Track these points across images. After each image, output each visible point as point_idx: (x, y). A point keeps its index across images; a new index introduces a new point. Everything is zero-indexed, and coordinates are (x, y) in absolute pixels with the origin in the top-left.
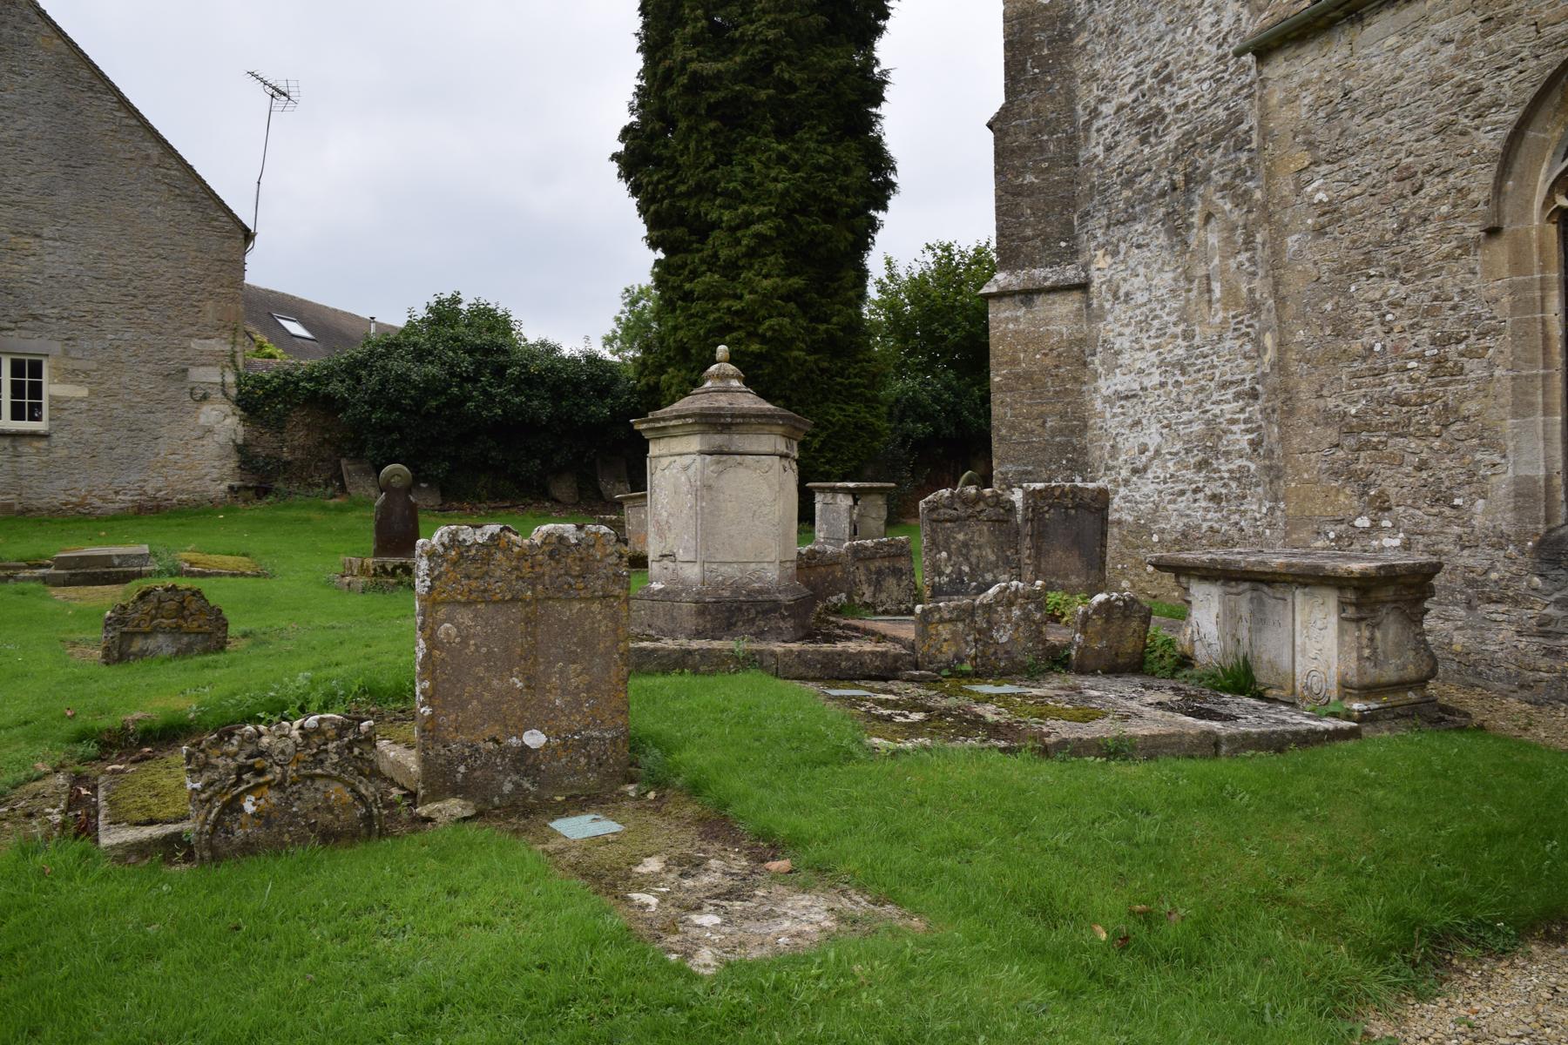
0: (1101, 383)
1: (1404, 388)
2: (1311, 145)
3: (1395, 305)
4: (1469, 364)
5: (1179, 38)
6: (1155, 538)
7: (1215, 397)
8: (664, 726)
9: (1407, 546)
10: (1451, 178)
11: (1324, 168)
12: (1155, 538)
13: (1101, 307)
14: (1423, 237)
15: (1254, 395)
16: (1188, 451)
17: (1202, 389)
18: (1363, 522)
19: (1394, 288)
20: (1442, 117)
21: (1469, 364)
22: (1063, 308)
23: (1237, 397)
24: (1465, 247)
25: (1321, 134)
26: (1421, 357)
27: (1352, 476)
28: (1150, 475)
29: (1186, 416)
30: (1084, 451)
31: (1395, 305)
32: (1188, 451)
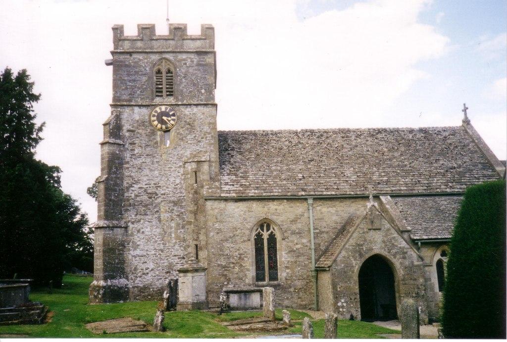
0: (131, 252)
1: (234, 261)
2: (216, 219)
3: (232, 248)
4: (245, 259)
5: (163, 179)
6: (151, 290)
7: (172, 258)
8: (402, 287)
9: (234, 287)
10: (243, 231)
11: (218, 223)
12: (151, 290)
13: (132, 233)
14: (237, 238)
15: (184, 258)
16: (163, 270)
17: (168, 256)
18: (226, 283)
19: (232, 245)
20: (242, 221)
21: (245, 259)
22: (119, 231)
23: (179, 258)
24: (244, 241)
25: (218, 217)
26: (237, 256)
27: (223, 275)
28: (149, 275)
29: (162, 262)
30: (123, 269)
31: (232, 248)
32: (163, 270)
